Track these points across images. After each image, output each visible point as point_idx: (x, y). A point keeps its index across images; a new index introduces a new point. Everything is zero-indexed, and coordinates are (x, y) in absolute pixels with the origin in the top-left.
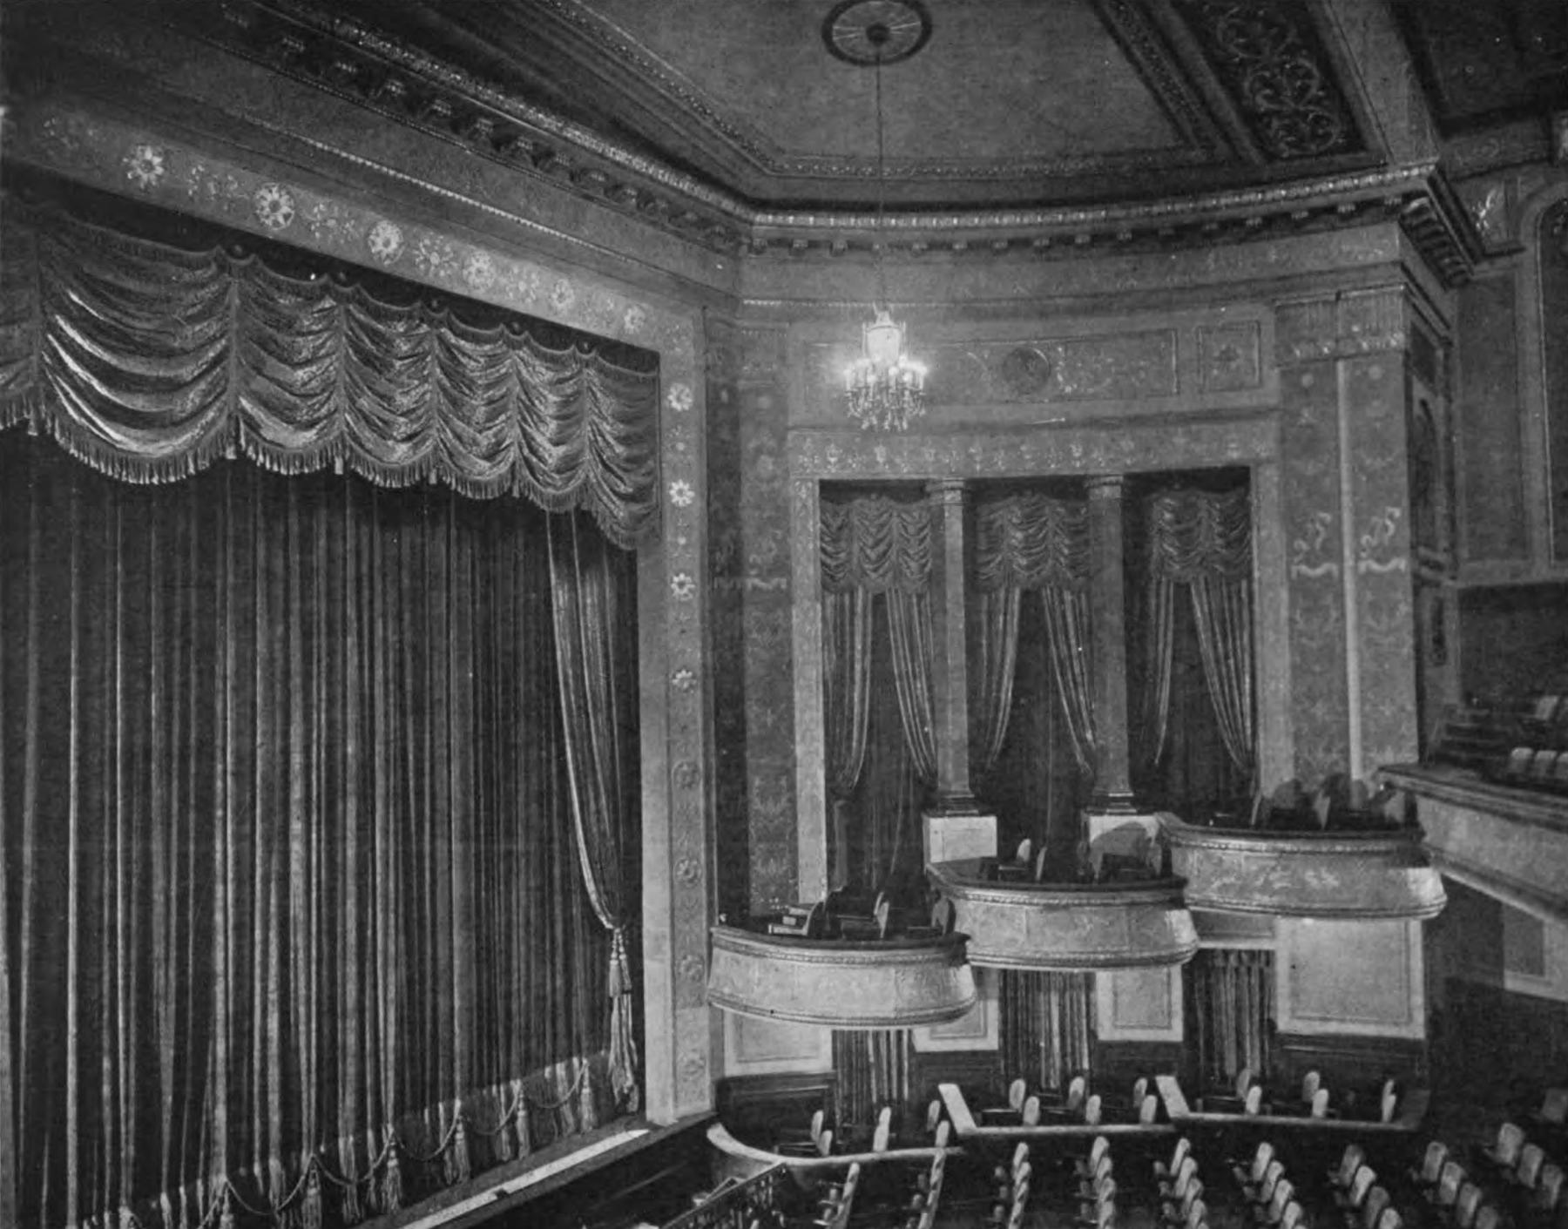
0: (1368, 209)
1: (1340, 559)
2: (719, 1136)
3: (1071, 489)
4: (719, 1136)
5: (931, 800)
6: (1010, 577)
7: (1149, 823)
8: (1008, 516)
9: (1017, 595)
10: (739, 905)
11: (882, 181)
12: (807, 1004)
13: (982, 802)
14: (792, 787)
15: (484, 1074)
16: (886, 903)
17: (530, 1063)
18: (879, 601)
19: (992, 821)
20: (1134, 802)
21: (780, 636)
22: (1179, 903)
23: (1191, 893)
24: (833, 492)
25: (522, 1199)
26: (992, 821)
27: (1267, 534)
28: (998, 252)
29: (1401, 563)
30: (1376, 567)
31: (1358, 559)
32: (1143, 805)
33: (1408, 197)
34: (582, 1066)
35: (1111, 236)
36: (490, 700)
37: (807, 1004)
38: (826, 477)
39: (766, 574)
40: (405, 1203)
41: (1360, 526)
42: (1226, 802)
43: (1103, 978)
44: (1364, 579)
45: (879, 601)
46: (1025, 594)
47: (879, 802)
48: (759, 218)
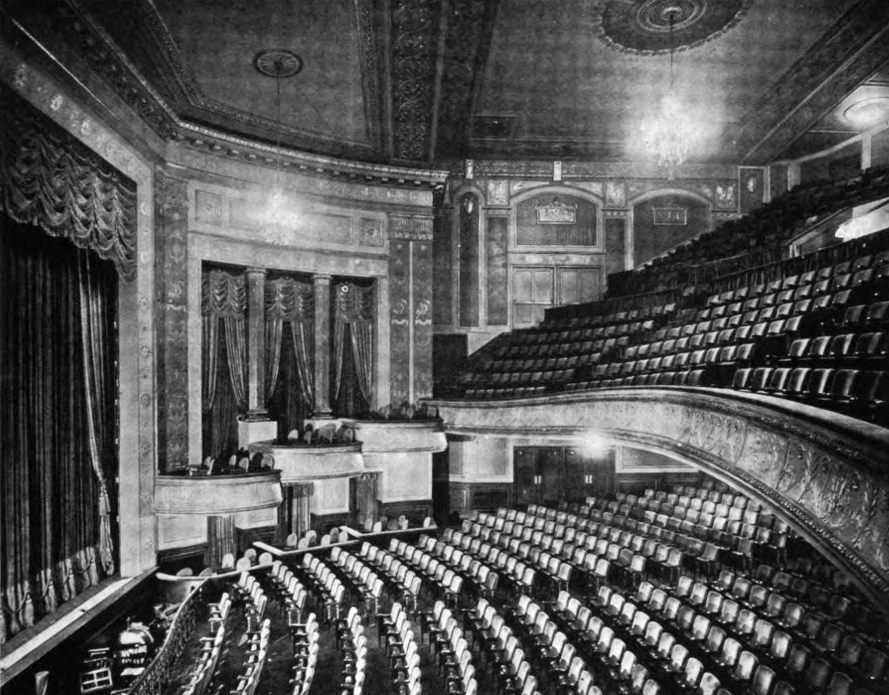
0: (426, 185)
1: (408, 319)
2: (161, 576)
3: (307, 278)
4: (161, 576)
5: (245, 413)
7: (338, 423)
8: (279, 285)
9: (281, 322)
12: (200, 506)
14: (186, 408)
15: (58, 557)
17: (73, 552)
18: (222, 320)
19: (275, 423)
20: (331, 414)
21: (182, 334)
22: (360, 451)
24: (207, 266)
25: (98, 612)
26: (275, 423)
27: (383, 304)
28: (335, 176)
29: (429, 322)
30: (421, 323)
31: (415, 318)
32: (335, 415)
33: (438, 183)
34: (91, 551)
35: (331, 172)
37: (200, 506)
38: (205, 258)
39: (177, 304)
42: (365, 413)
44: (416, 327)
45: (222, 320)
46: (284, 323)
47: (222, 415)
48: (182, 124)
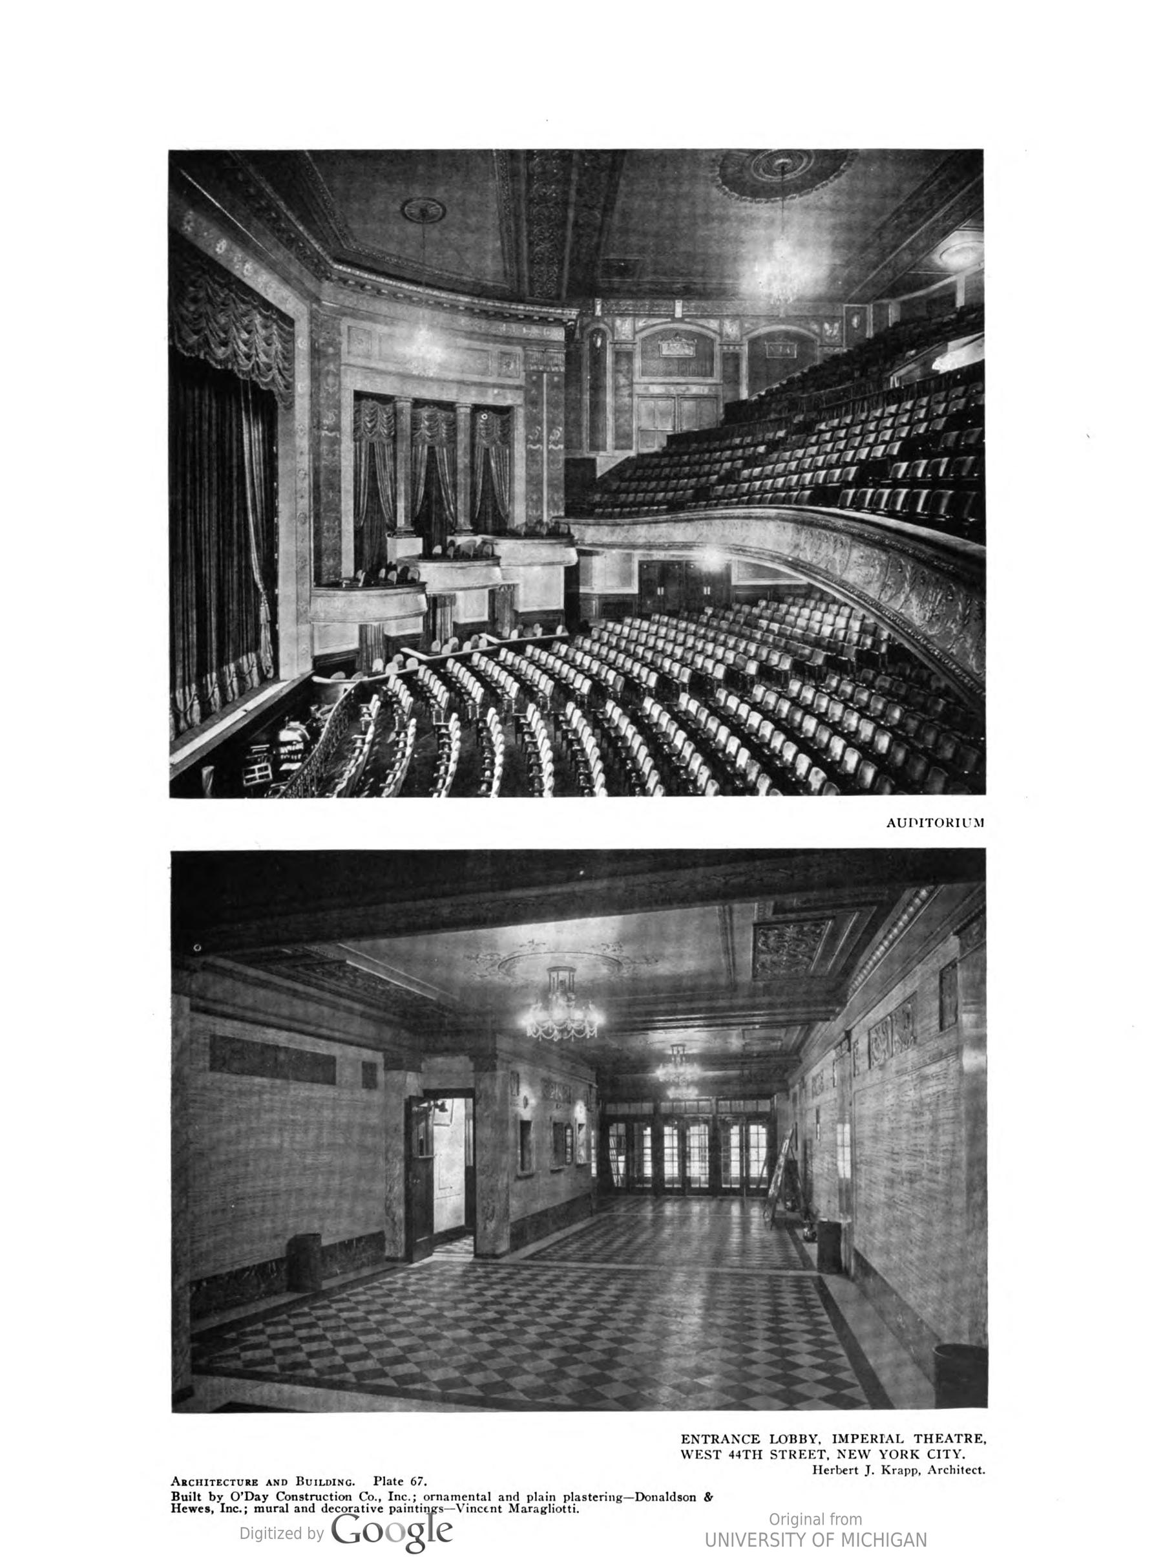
3: (450, 407)
6: (424, 442)
7: (478, 539)
8: (425, 413)
10: (326, 579)
11: (423, 247)
13: (418, 533)
15: (222, 662)
16: (375, 572)
17: (236, 657)
18: (372, 445)
22: (498, 565)
23: (502, 562)
24: (359, 396)
29: (561, 447)
32: (476, 532)
34: (252, 656)
36: (374, 493)
39: (331, 430)
40: (202, 721)
41: (550, 432)
42: (503, 530)
43: (459, 594)
44: (550, 452)
45: (372, 445)
